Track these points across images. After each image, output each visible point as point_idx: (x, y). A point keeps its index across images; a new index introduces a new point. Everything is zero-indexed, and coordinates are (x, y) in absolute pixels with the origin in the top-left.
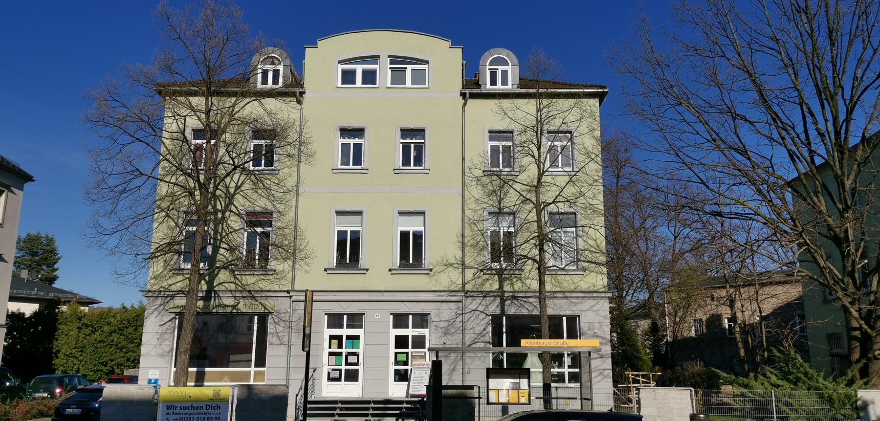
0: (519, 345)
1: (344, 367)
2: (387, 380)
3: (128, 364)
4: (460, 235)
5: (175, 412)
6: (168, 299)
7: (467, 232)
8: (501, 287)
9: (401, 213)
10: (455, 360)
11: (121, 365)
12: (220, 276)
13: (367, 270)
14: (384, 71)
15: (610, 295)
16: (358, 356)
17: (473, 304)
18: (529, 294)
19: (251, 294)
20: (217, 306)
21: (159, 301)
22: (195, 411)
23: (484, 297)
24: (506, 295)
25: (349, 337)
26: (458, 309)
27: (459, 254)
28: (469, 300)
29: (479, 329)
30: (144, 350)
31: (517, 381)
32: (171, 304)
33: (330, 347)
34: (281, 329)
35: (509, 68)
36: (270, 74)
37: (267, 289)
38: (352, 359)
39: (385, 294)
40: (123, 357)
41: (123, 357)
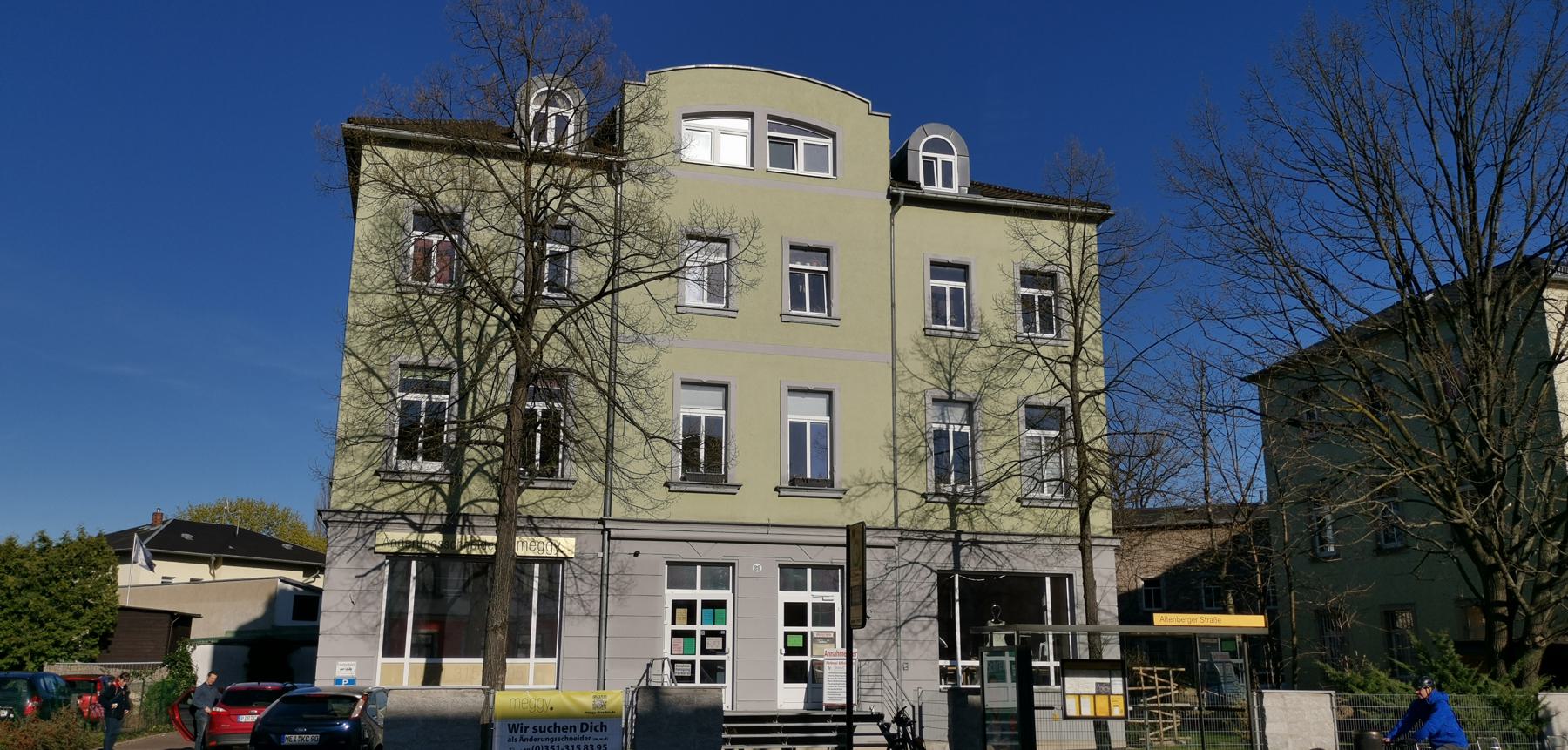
0: (1150, 622)
1: (698, 658)
2: (775, 680)
3: (54, 651)
4: (889, 435)
5: (525, 735)
6: (373, 527)
7: (900, 431)
8: (954, 525)
9: (792, 391)
10: (886, 646)
11: (42, 654)
12: (471, 487)
13: (739, 486)
15: (1117, 542)
16: (724, 637)
17: (910, 552)
18: (997, 538)
20: (468, 544)
21: (354, 532)
22: (562, 734)
23: (930, 540)
24: (964, 537)
25: (707, 604)
26: (889, 559)
27: (889, 467)
28: (904, 545)
29: (920, 595)
30: (325, 623)
31: (1106, 680)
32: (381, 537)
33: (674, 622)
34: (586, 588)
35: (954, 159)
36: (552, 123)
37: (560, 514)
38: (713, 643)
39: (772, 530)
40: (45, 638)
41: (45, 638)
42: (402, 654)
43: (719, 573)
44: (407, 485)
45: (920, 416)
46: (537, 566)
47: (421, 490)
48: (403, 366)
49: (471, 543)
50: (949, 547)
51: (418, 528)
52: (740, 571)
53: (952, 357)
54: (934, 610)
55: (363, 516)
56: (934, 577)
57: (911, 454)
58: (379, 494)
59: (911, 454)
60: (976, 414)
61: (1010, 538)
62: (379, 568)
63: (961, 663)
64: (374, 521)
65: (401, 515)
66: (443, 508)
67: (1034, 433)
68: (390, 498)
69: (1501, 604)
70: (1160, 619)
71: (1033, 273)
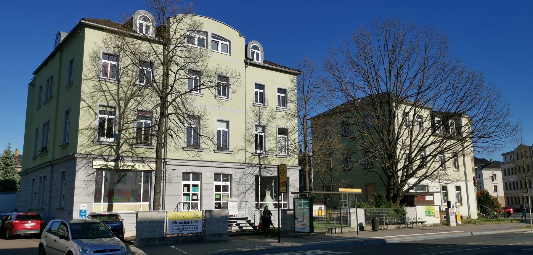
0: (339, 191)
6: (91, 160)
8: (260, 162)
9: (218, 121)
12: (123, 147)
17: (249, 170)
18: (271, 166)
20: (123, 166)
21: (85, 161)
22: (186, 224)
24: (263, 166)
25: (193, 186)
29: (251, 183)
30: (76, 191)
32: (95, 163)
35: (259, 52)
37: (150, 157)
38: (195, 197)
42: (100, 202)
43: (197, 176)
44: (102, 146)
45: (251, 130)
46: (143, 173)
47: (106, 148)
48: (100, 106)
49: (123, 166)
50: (258, 169)
51: (106, 160)
52: (203, 175)
53: (260, 113)
54: (254, 187)
55: (89, 156)
56: (254, 178)
57: (249, 141)
58: (91, 149)
59: (249, 141)
60: (266, 130)
62: (93, 173)
63: (260, 202)
64: (92, 158)
65: (101, 156)
66: (114, 153)
67: (280, 136)
68: (96, 150)
69: (392, 185)
70: (341, 190)
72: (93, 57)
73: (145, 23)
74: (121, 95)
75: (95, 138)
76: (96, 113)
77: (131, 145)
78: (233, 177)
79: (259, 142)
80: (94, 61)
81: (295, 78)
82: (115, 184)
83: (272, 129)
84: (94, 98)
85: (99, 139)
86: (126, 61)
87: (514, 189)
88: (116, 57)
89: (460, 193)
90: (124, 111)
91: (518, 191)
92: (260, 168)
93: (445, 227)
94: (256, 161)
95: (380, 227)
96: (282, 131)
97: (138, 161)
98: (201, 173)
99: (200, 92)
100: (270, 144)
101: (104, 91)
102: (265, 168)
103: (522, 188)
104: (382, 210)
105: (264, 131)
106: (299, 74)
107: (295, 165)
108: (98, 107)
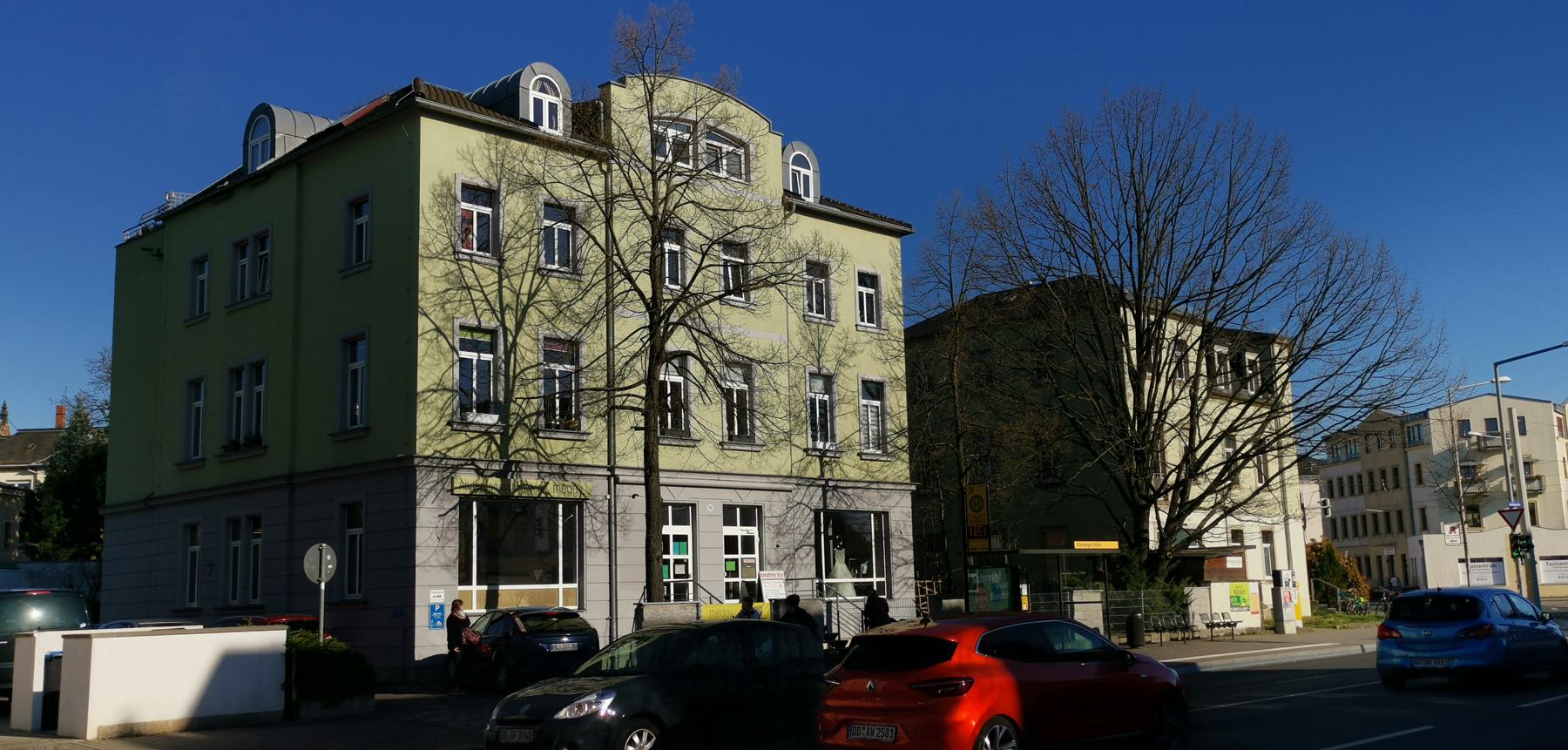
8: (822, 474)
14: (1535, 485)
17: (800, 495)
19: (563, 471)
20: (520, 487)
21: (435, 476)
29: (804, 528)
30: (420, 557)
35: (809, 173)
38: (680, 569)
48: (462, 328)
49: (520, 487)
50: (820, 491)
52: (700, 510)
54: (812, 541)
58: (449, 443)
60: (835, 386)
61: (855, 484)
66: (496, 456)
67: (864, 402)
68: (459, 446)
71: (477, 188)
72: (440, 196)
73: (547, 99)
74: (508, 296)
75: (454, 413)
76: (453, 348)
77: (534, 432)
78: (766, 513)
79: (821, 421)
80: (444, 205)
81: (896, 242)
82: (515, 532)
83: (849, 385)
84: (448, 306)
85: (463, 418)
86: (514, 207)
87: (1356, 534)
88: (487, 195)
89: (1272, 549)
90: (515, 344)
91: (1365, 541)
92: (825, 489)
93: (1271, 636)
94: (814, 471)
95: (1147, 639)
96: (873, 390)
97: (551, 474)
98: (694, 506)
99: (748, 299)
100: (845, 425)
101: (468, 288)
102: (835, 488)
103: (1377, 531)
104: (1138, 595)
105: (828, 389)
106: (907, 233)
107: (902, 479)
108: (457, 330)
